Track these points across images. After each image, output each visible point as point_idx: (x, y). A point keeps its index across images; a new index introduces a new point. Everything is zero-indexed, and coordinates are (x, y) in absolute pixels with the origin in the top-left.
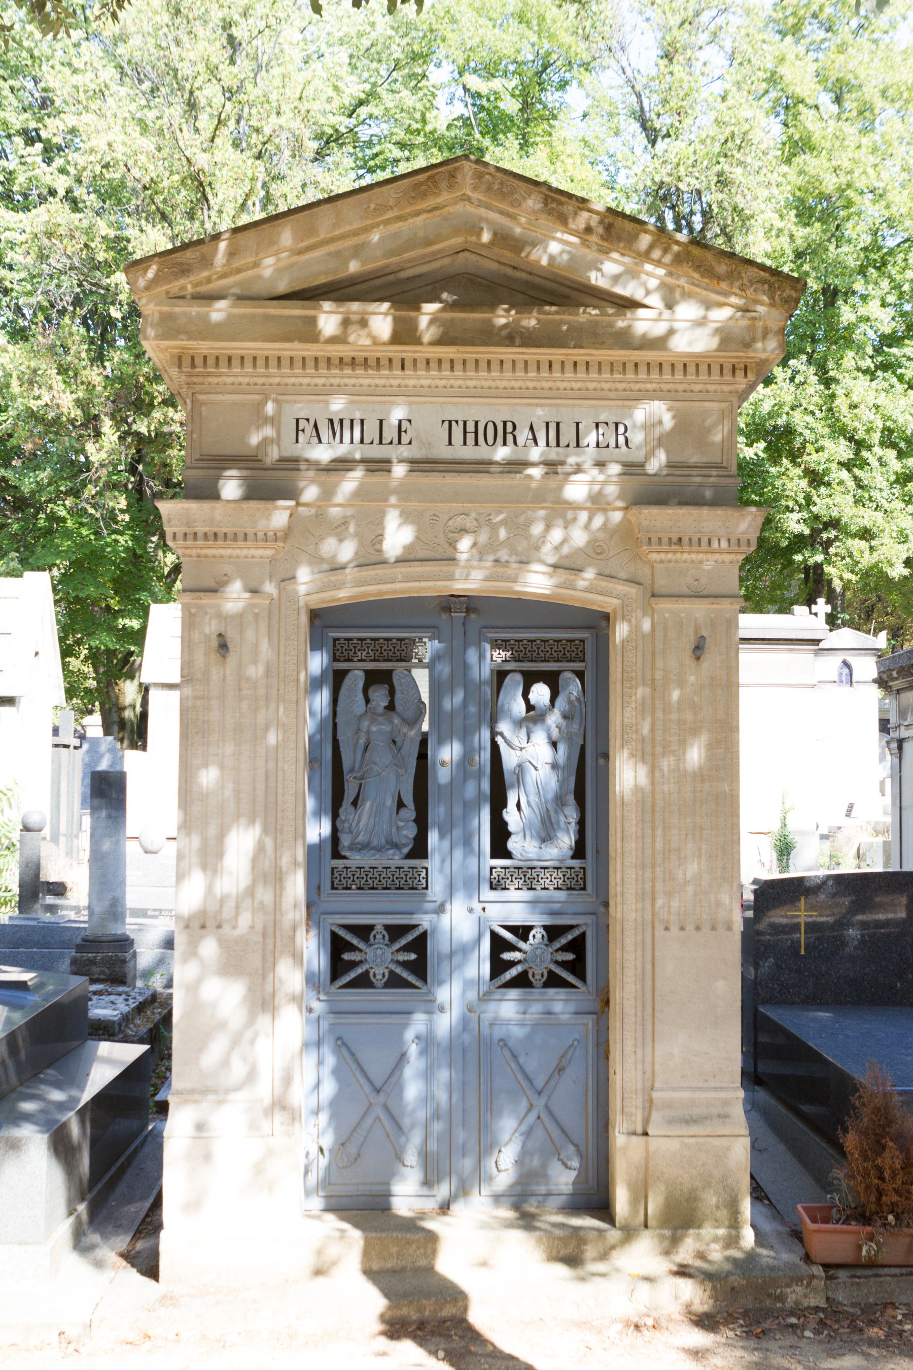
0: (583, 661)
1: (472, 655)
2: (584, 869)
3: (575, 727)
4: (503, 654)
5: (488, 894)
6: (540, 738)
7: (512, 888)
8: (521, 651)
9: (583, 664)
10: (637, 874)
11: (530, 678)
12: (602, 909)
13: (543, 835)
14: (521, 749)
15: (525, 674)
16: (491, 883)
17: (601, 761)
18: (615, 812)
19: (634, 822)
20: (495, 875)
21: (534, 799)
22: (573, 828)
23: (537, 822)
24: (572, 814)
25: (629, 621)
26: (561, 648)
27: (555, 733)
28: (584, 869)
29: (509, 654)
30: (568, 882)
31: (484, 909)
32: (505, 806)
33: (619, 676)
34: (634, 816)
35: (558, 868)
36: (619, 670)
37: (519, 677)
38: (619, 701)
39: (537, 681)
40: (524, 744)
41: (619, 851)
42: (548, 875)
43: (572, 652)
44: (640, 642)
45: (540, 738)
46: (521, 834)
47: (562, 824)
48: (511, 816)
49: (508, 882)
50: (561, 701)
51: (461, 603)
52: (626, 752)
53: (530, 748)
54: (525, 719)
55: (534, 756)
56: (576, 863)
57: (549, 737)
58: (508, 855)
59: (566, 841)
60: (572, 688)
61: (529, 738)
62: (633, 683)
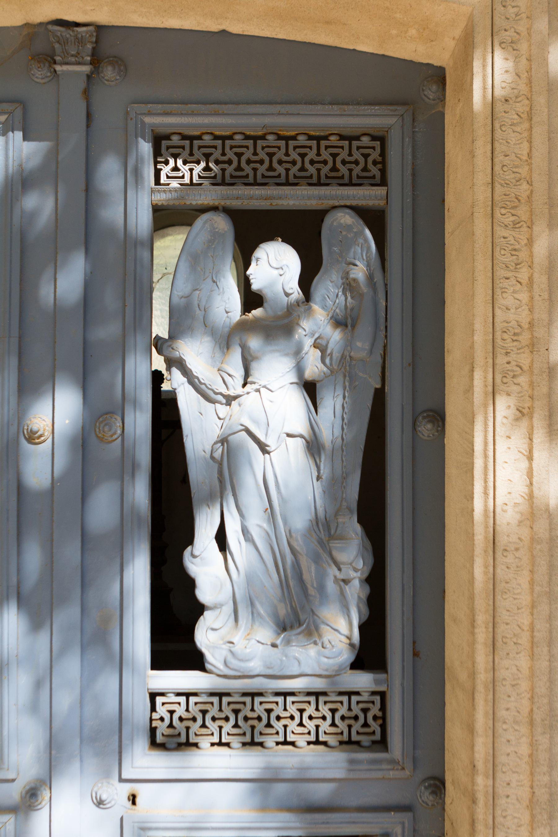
0: (383, 182)
1: (109, 171)
2: (383, 695)
3: (362, 346)
4: (185, 169)
5: (144, 761)
6: (277, 374)
7: (205, 743)
8: (232, 159)
9: (381, 191)
10: (533, 744)
11: (250, 232)
12: (427, 797)
13: (283, 611)
14: (230, 400)
15: (237, 216)
16: (153, 731)
17: (426, 429)
18: (468, 572)
19: (525, 599)
20: (162, 711)
21: (257, 522)
22: (356, 590)
23: (270, 583)
24: (353, 558)
25: (510, 46)
26: (325, 155)
27: (314, 366)
28: (383, 695)
29: (198, 169)
30: (342, 726)
31: (133, 799)
32: (189, 539)
33: (482, 194)
34: (524, 580)
35: (317, 694)
36: (482, 178)
37: (223, 224)
38: (482, 264)
39: (270, 238)
40: (235, 388)
41: (482, 677)
42: (293, 710)
43: (360, 160)
44: (541, 100)
45: (277, 374)
46: (228, 608)
47: (331, 587)
48: (205, 565)
49: (195, 727)
50: (328, 288)
51: (80, 41)
52: (504, 407)
53: (250, 400)
54: (242, 327)
55: (266, 421)
56: (363, 681)
57: (299, 370)
58: (195, 661)
59: (341, 629)
60: (356, 254)
61: (247, 374)
62: (523, 212)
